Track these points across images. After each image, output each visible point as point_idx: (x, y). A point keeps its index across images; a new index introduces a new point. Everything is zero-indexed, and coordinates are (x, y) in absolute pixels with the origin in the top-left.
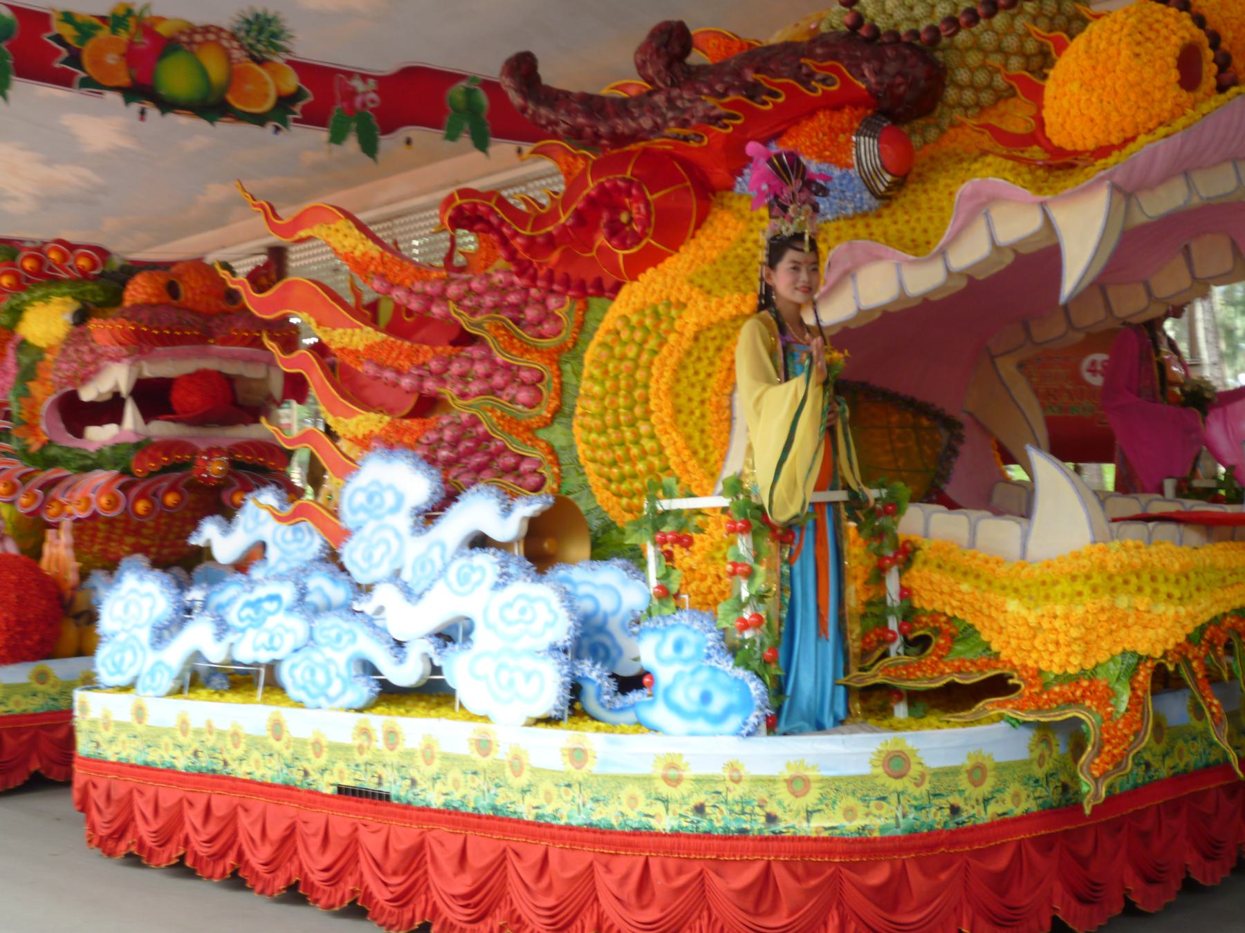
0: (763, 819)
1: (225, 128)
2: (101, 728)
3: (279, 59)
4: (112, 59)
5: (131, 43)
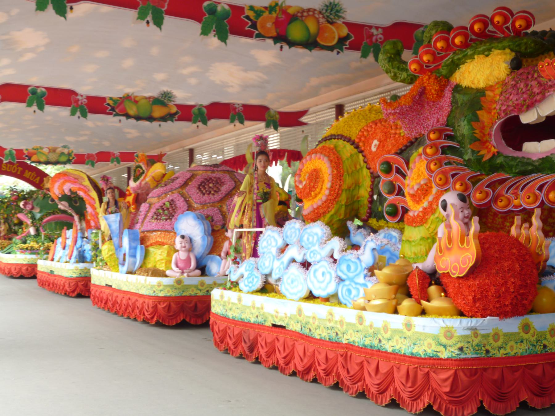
0: (485, 352)
1: (316, 53)
2: (227, 304)
3: (340, 22)
4: (269, 25)
5: (277, 18)
